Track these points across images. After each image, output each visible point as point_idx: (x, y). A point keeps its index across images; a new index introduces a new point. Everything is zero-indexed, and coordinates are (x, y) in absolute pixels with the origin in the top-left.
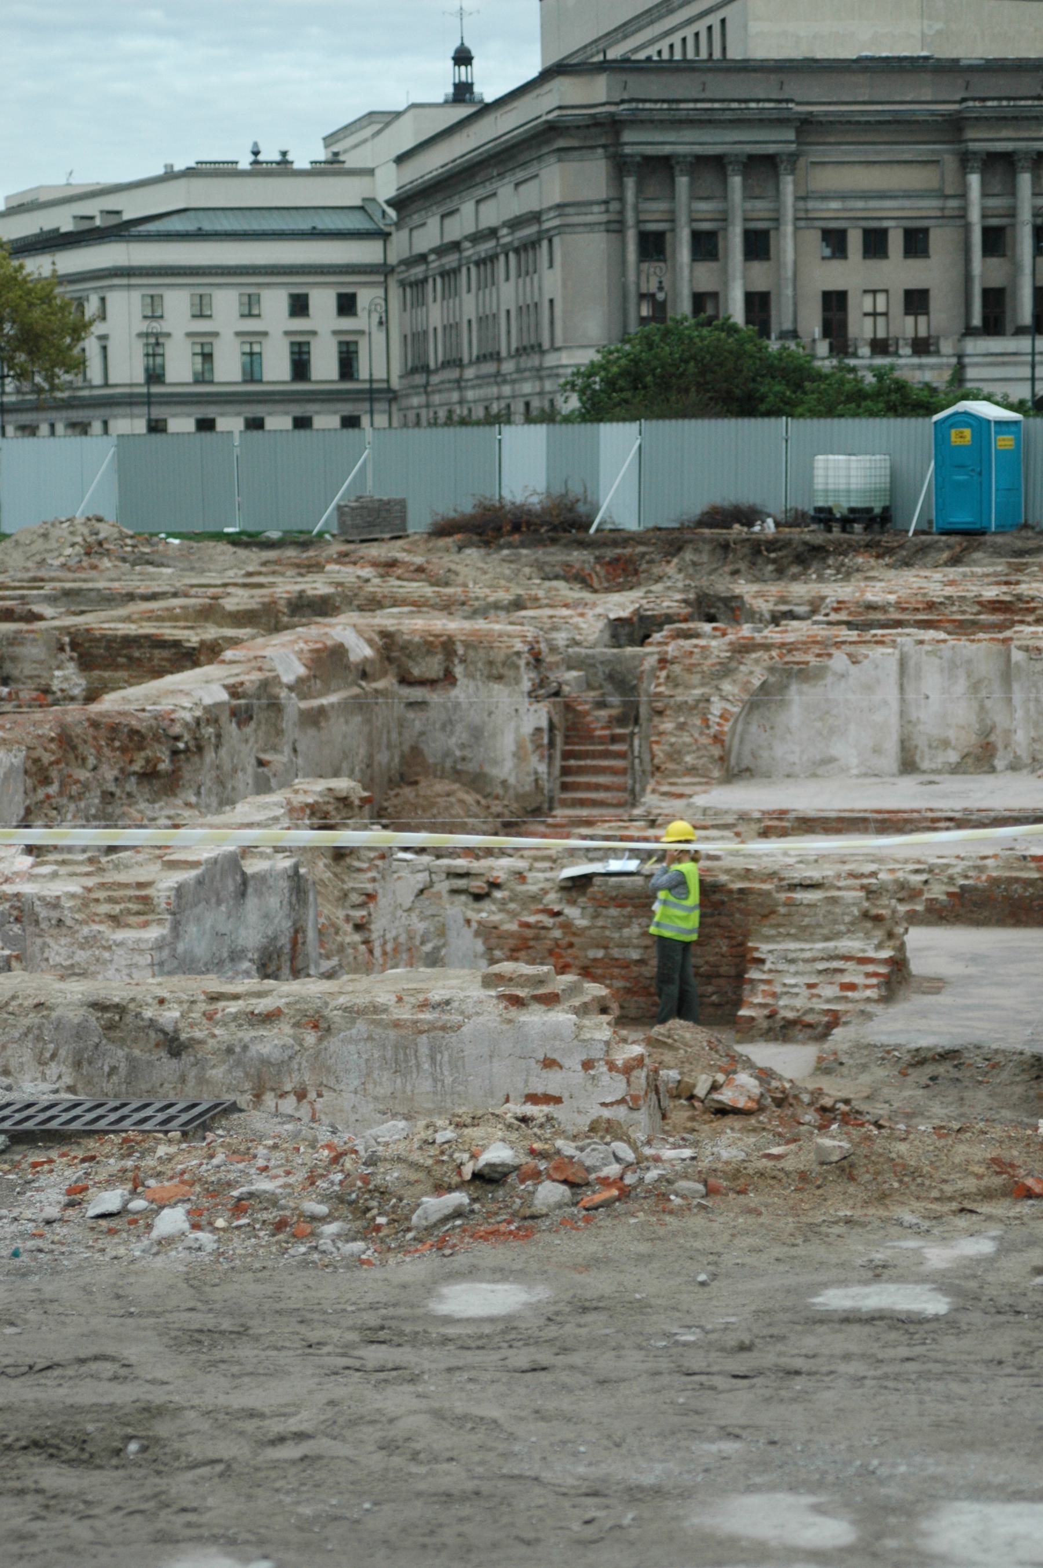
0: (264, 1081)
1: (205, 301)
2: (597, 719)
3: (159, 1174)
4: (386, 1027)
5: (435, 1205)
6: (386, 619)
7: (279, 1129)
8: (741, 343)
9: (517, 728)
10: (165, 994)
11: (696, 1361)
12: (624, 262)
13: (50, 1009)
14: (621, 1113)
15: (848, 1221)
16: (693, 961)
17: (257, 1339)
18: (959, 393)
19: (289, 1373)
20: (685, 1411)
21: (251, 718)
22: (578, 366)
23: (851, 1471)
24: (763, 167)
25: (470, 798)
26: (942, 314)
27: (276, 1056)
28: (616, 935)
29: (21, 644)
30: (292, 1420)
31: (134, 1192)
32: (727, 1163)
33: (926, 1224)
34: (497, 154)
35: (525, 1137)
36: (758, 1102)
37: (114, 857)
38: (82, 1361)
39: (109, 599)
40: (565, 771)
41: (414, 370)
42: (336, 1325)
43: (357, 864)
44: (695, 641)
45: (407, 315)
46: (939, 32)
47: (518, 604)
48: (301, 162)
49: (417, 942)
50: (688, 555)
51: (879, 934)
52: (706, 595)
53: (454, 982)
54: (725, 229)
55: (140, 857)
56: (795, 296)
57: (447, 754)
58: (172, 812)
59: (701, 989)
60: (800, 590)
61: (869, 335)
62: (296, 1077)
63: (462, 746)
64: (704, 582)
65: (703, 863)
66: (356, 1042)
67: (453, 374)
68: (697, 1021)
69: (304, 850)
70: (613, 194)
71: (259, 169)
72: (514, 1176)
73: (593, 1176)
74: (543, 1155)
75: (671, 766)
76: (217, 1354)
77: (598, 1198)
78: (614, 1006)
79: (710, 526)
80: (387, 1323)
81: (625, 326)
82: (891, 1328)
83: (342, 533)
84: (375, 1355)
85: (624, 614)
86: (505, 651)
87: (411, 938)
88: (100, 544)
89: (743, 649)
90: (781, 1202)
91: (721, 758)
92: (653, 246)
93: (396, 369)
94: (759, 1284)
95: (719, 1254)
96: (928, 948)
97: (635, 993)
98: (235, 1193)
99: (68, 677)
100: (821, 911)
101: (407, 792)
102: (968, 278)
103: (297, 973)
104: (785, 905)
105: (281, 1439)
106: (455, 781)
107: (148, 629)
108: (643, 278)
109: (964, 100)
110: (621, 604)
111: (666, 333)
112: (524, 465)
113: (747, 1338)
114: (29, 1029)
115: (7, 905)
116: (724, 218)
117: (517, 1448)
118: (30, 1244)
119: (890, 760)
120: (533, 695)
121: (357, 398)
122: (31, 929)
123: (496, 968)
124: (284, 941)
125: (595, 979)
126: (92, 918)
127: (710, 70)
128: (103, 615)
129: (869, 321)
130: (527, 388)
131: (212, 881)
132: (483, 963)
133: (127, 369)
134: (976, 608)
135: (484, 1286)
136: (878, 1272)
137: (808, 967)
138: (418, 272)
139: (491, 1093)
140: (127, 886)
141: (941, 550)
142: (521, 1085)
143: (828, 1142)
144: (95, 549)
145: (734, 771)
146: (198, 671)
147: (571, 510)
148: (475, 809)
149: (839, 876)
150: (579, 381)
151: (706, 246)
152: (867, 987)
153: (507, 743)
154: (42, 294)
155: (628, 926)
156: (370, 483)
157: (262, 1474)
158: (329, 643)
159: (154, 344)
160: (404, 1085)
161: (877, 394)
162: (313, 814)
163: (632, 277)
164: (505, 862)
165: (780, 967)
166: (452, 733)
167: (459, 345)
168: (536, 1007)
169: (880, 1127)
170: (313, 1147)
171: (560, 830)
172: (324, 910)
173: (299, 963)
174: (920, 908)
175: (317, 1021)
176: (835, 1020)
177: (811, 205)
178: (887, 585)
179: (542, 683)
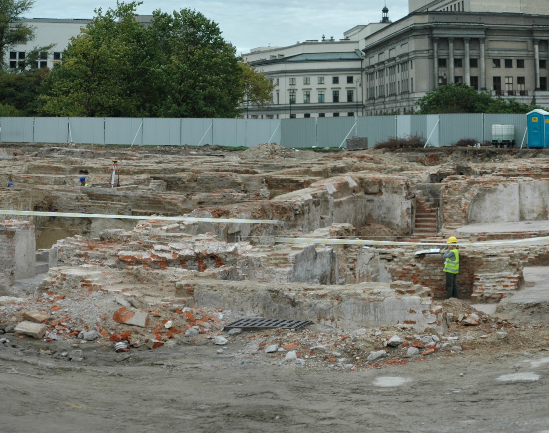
0: (321, 315)
1: (308, 79)
2: (426, 205)
3: (288, 341)
4: (360, 300)
5: (375, 354)
6: (361, 174)
7: (325, 330)
8: (469, 91)
9: (402, 208)
10: (291, 288)
11: (460, 398)
12: (434, 67)
13: (256, 291)
14: (435, 326)
15: (507, 356)
16: (457, 280)
17: (317, 390)
18: (534, 107)
19: (327, 401)
20: (456, 412)
21: (319, 204)
22: (420, 98)
23: (510, 425)
24: (475, 41)
25: (387, 230)
26: (528, 84)
27: (325, 308)
28: (433, 272)
29: (251, 181)
30: (328, 414)
31: (280, 346)
32: (469, 340)
33: (531, 355)
34: (395, 37)
35: (404, 334)
36: (478, 322)
37: (277, 246)
38: (262, 393)
39: (277, 168)
40: (417, 221)
41: (370, 99)
42: (343, 388)
43: (351, 250)
44: (456, 181)
45: (368, 83)
46: (525, 7)
47: (402, 170)
48: (337, 40)
49: (370, 274)
50: (454, 155)
51: (515, 270)
52: (460, 167)
53: (381, 287)
54: (464, 58)
55: (284, 246)
56: (485, 78)
57: (380, 216)
58: (294, 233)
59: (460, 288)
60: (489, 165)
61: (507, 89)
62: (331, 314)
63: (384, 214)
64: (459, 163)
65: (460, 249)
66: (350, 304)
67: (382, 100)
68: (459, 298)
69: (335, 245)
70: (430, 48)
71: (324, 42)
72: (400, 345)
73: (426, 345)
74: (410, 339)
75: (449, 219)
76: (305, 394)
77: (427, 352)
78: (432, 294)
79: (461, 146)
80: (359, 388)
81: (434, 86)
82: (521, 385)
83: (348, 148)
84: (355, 397)
85: (435, 172)
86: (397, 184)
87: (368, 273)
88: (275, 151)
89: (471, 183)
90: (486, 351)
91: (465, 217)
92: (443, 63)
93: (365, 99)
94: (480, 375)
95: (467, 367)
96: (530, 273)
97: (439, 290)
98: (311, 348)
99: (265, 191)
100: (497, 263)
101: (367, 228)
102: (536, 74)
103: (332, 283)
104: (486, 262)
105: (324, 419)
106: (382, 224)
107: (288, 177)
108: (440, 72)
109: (533, 25)
110: (434, 169)
111: (447, 88)
112: (404, 127)
113: (476, 391)
114: (250, 298)
115: (244, 260)
116: (464, 55)
117: (401, 423)
118: (247, 360)
119: (517, 217)
120: (406, 198)
121: (353, 107)
122: (251, 267)
123: (395, 282)
124: (328, 273)
125: (426, 285)
126: (270, 264)
127: (459, 14)
128: (275, 172)
129: (507, 85)
130: (405, 104)
131: (306, 253)
132: (391, 281)
133: (285, 100)
134: (541, 170)
135: (391, 377)
136: (517, 370)
137: (493, 281)
138: (371, 70)
139: (393, 321)
140: (280, 255)
141: (530, 153)
142: (403, 318)
143: (500, 333)
144: (273, 153)
145: (469, 221)
146: (303, 190)
147: (418, 141)
148: (388, 233)
149: (502, 252)
150: (420, 102)
151: (458, 63)
152: (511, 286)
153: (398, 213)
154: (260, 78)
155: (437, 269)
156: (356, 133)
157: (318, 428)
158: (343, 181)
159: (293, 92)
160: (365, 318)
161: (510, 107)
162: (338, 234)
163: (436, 72)
164: (397, 249)
165: (484, 281)
166: (381, 209)
167: (384, 91)
168: (407, 294)
169: (516, 327)
170: (336, 336)
171: (415, 240)
172: (340, 264)
173: (333, 280)
174: (527, 261)
175: (338, 298)
176: (502, 296)
177: (489, 52)
178: (514, 164)
179: (409, 194)
